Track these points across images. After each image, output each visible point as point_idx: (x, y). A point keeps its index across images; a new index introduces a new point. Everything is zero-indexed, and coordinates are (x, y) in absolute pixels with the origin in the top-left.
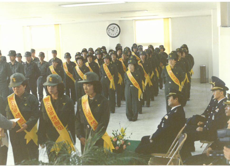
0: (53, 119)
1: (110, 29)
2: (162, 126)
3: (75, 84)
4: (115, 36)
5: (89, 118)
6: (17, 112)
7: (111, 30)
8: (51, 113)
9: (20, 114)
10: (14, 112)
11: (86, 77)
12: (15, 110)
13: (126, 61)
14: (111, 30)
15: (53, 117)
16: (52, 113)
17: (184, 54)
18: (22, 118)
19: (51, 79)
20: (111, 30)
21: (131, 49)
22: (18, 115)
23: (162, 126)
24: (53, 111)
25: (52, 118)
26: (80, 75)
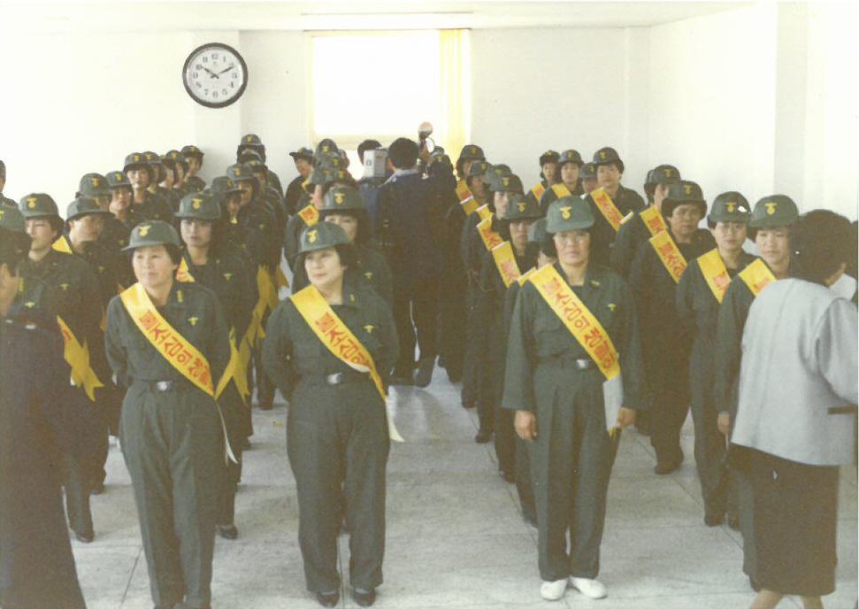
0: (590, 340)
1: (199, 67)
2: (180, 299)
3: (288, 225)
4: (222, 98)
5: (576, 325)
6: (591, 328)
7: (207, 70)
8: (579, 324)
9: (598, 332)
10: (578, 327)
11: (200, 203)
12: (579, 321)
13: (134, 179)
14: (205, 72)
15: (591, 335)
16: (582, 323)
17: (501, 202)
18: (605, 342)
19: (569, 211)
20: (207, 70)
21: (454, 161)
22: (591, 337)
23: (180, 299)
24: (585, 316)
25: (587, 337)
26: (611, 218)
